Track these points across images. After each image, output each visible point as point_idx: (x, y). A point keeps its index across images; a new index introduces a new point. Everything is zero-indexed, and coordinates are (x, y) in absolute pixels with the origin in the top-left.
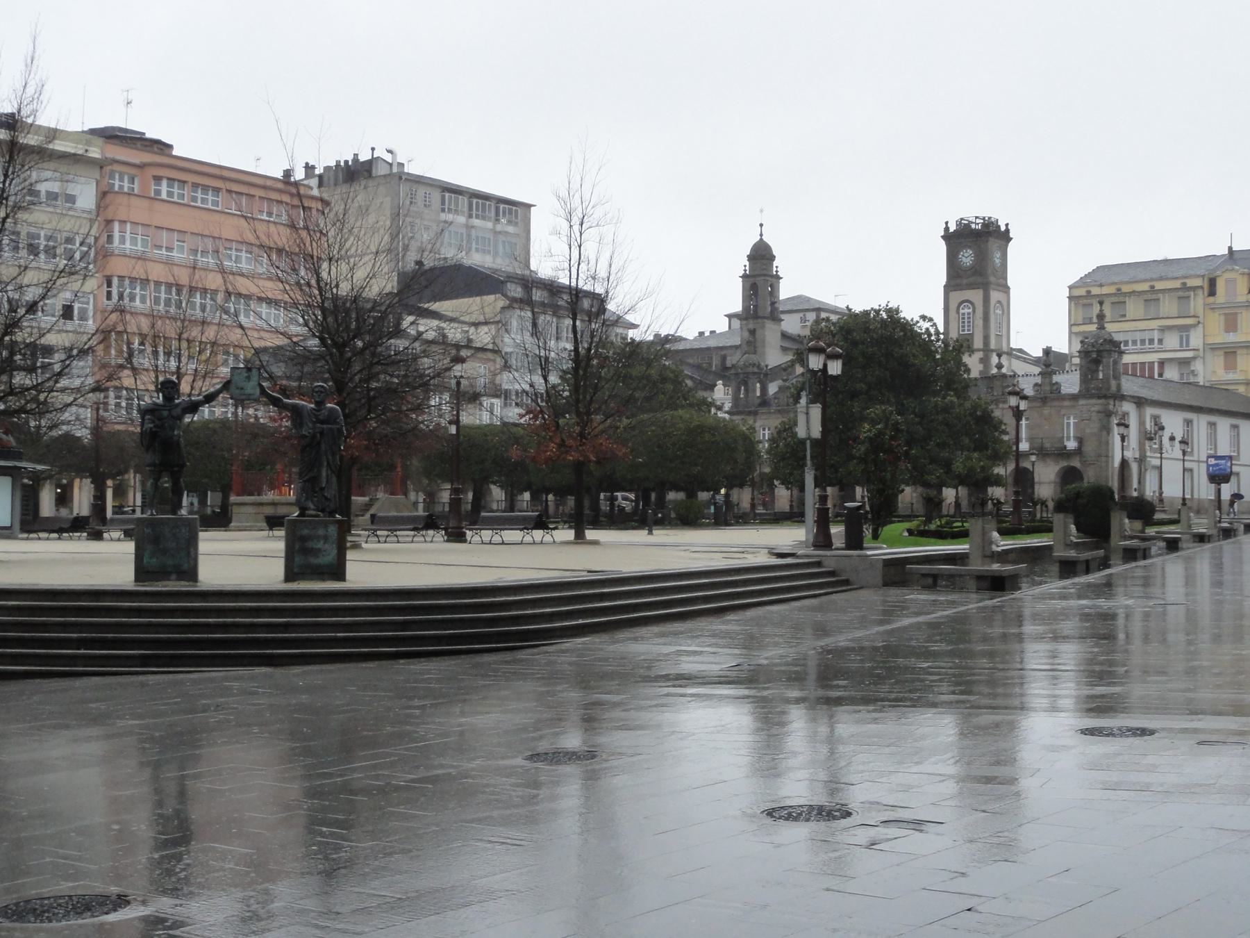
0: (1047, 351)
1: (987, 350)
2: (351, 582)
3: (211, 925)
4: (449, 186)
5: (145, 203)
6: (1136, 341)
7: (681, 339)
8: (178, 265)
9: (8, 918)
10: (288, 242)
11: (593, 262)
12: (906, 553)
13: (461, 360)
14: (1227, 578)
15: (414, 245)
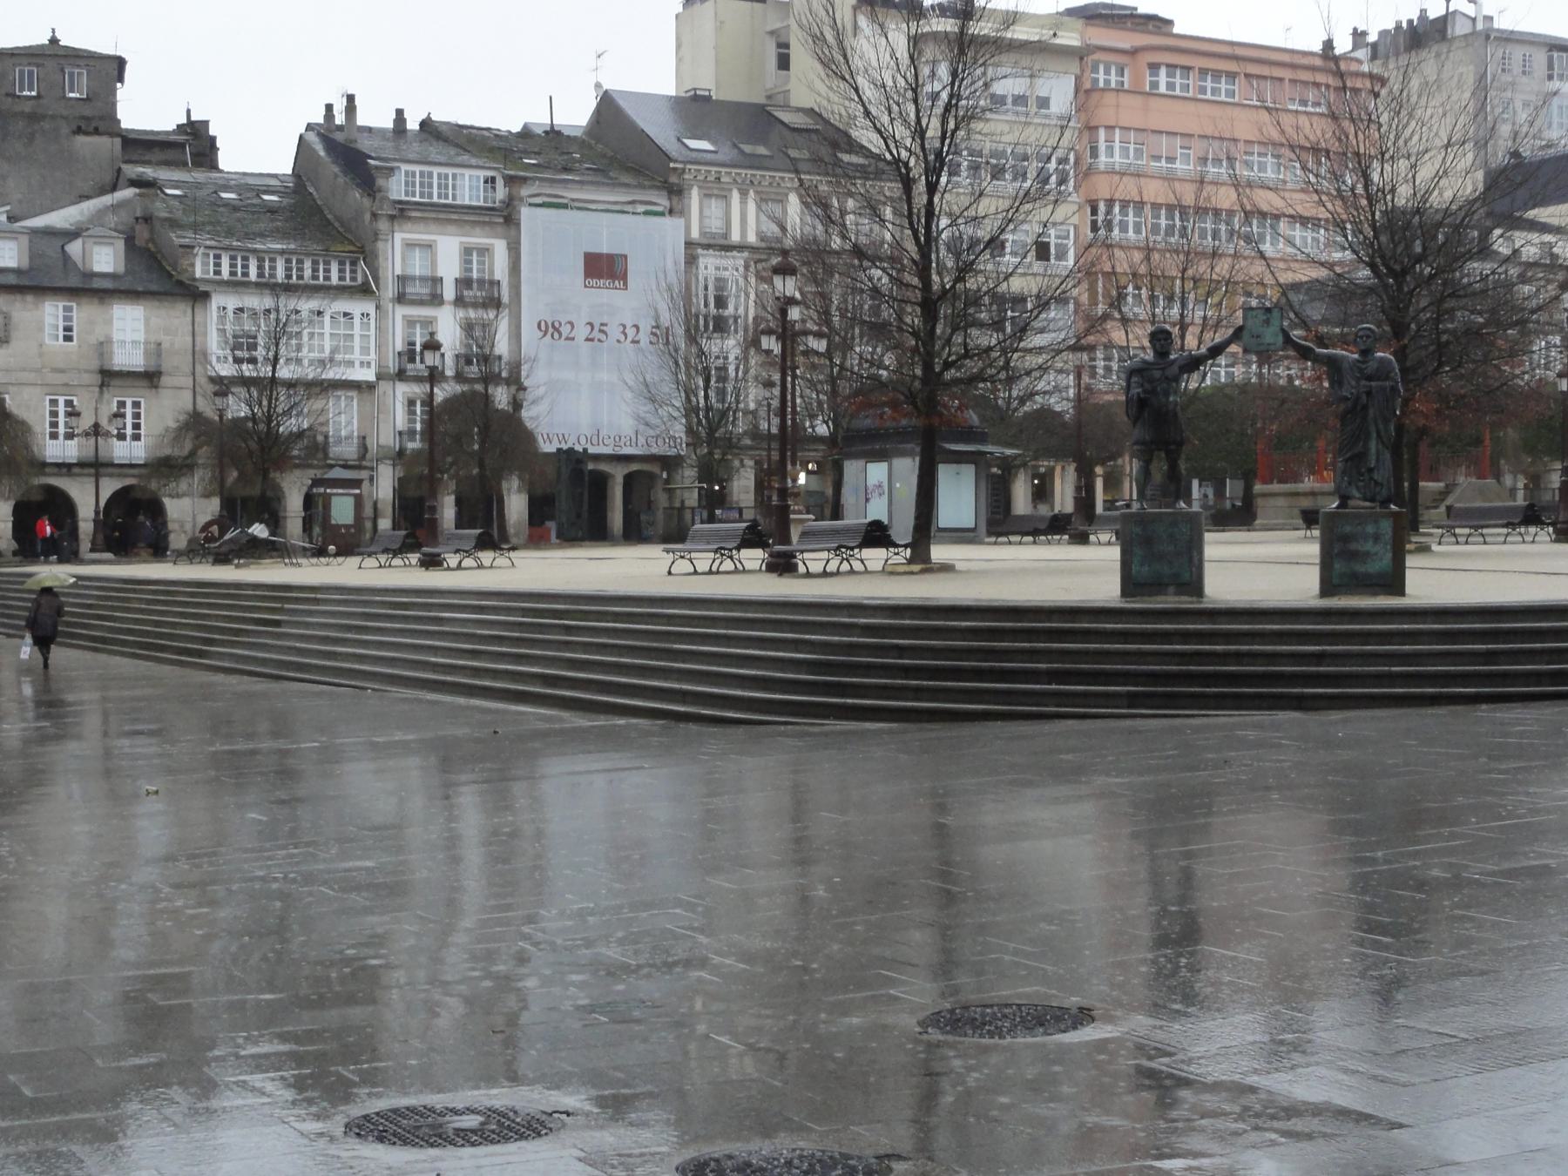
3: (1199, 1058)
5: (1136, 101)
8: (1180, 180)
9: (940, 1028)
15: (1505, 130)
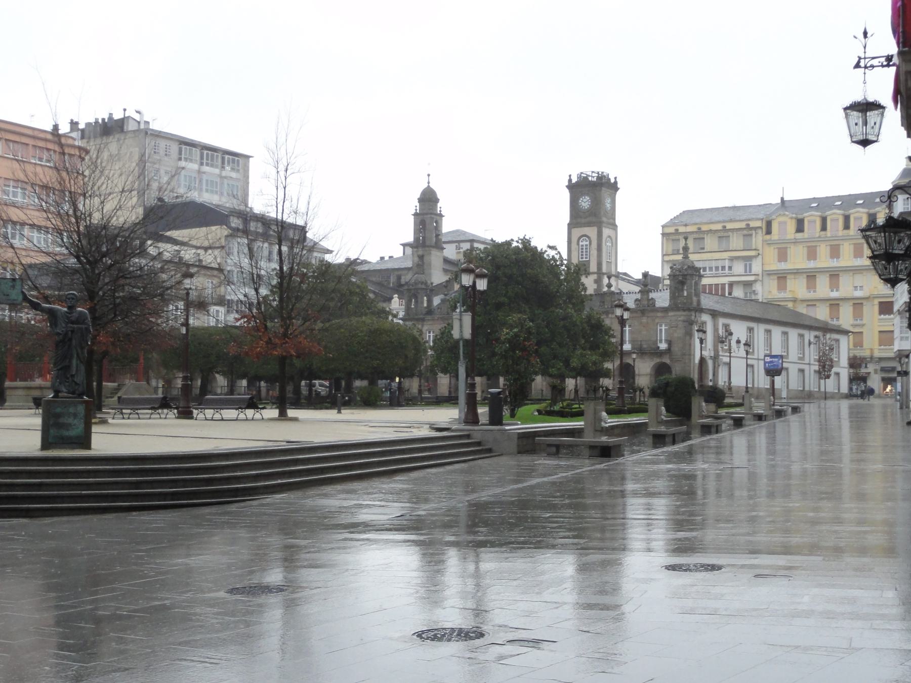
0: (645, 275)
1: (600, 273)
2: (95, 450)
4: (184, 140)
6: (712, 267)
7: (365, 262)
10: (51, 180)
11: (295, 201)
12: (535, 428)
13: (191, 276)
14: (779, 447)
15: (155, 185)
